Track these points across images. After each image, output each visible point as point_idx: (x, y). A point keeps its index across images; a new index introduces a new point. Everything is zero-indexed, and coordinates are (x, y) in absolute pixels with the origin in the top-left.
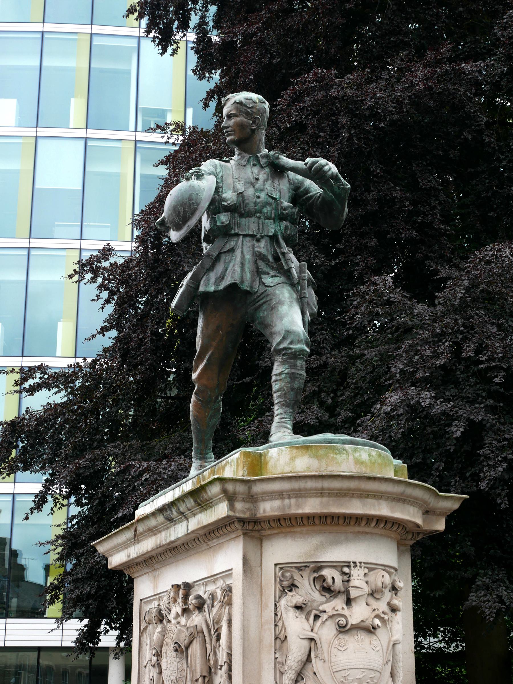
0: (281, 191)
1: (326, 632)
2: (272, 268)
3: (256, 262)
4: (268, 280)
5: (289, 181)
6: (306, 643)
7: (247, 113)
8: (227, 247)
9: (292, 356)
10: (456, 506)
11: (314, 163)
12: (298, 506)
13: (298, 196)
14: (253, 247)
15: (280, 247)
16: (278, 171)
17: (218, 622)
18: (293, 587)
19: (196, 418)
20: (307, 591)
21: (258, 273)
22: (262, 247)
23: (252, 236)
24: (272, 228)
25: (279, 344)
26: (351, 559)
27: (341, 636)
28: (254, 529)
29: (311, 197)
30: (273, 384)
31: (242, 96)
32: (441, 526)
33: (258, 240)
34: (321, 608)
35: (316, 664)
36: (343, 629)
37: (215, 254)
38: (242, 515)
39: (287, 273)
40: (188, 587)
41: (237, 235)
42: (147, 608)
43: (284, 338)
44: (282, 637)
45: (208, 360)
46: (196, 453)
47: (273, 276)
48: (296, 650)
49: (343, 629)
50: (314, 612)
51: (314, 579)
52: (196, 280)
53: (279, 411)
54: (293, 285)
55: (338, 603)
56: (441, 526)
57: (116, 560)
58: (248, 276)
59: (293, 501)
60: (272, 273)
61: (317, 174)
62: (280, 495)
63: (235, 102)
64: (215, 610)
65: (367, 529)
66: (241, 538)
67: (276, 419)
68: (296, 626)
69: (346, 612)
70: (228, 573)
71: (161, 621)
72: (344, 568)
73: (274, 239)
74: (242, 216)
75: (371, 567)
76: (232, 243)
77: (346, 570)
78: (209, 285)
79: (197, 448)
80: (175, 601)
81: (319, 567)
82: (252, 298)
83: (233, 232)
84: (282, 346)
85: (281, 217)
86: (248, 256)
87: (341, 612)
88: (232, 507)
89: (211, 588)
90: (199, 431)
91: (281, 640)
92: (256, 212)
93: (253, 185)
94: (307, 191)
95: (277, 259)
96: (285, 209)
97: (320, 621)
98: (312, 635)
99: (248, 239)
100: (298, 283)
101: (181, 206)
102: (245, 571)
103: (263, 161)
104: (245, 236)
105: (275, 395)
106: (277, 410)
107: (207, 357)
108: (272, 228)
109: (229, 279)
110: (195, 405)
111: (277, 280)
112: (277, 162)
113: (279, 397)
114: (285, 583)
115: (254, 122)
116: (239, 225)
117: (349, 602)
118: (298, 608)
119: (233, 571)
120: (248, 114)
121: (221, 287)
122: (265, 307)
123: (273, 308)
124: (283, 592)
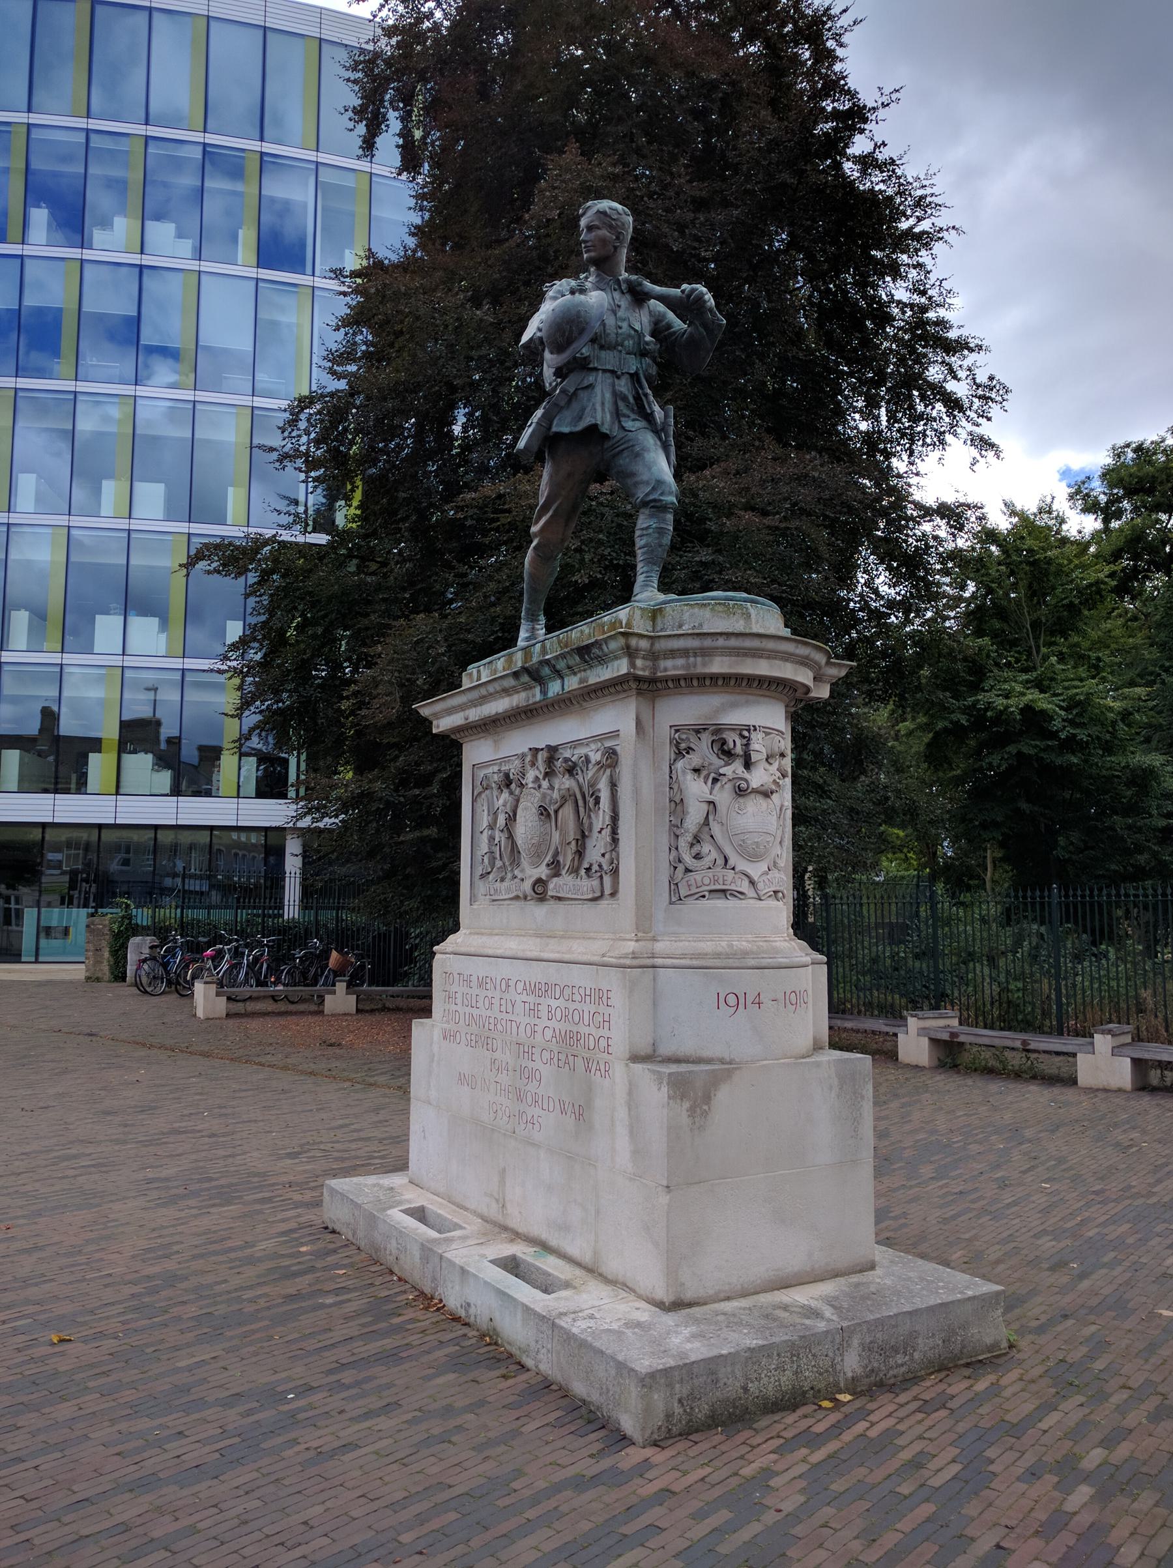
0: (641, 321)
1: (723, 796)
2: (633, 411)
3: (616, 403)
4: (629, 424)
5: (650, 312)
6: (705, 807)
7: (611, 226)
8: (586, 383)
10: (843, 673)
11: (693, 290)
12: (704, 665)
13: (659, 329)
14: (613, 385)
15: (642, 388)
16: (639, 297)
17: (592, 785)
18: (689, 750)
19: (531, 575)
20: (703, 751)
21: (617, 415)
22: (623, 386)
23: (613, 372)
24: (633, 365)
25: (647, 495)
26: (751, 723)
27: (741, 800)
28: (649, 687)
29: (675, 333)
30: (637, 540)
31: (605, 204)
33: (618, 378)
34: (721, 771)
37: (572, 390)
38: (641, 673)
39: (649, 417)
40: (552, 750)
41: (596, 369)
42: (481, 774)
43: (654, 489)
44: (678, 800)
45: (555, 511)
46: (527, 613)
47: (634, 420)
49: (741, 792)
50: (712, 775)
51: (713, 742)
52: (548, 418)
53: (645, 569)
55: (737, 768)
57: (442, 725)
59: (699, 659)
60: (633, 416)
61: (682, 307)
62: (685, 653)
63: (598, 211)
64: (590, 774)
65: (768, 693)
66: (634, 698)
67: (640, 579)
68: (696, 789)
69: (746, 775)
70: (615, 734)
71: (508, 786)
72: (743, 733)
73: (634, 377)
74: (602, 347)
76: (591, 379)
77: (746, 733)
78: (563, 426)
79: (528, 610)
80: (533, 764)
81: (718, 730)
82: (611, 443)
83: (591, 366)
84: (651, 497)
85: (643, 353)
86: (608, 396)
87: (742, 775)
88: (632, 665)
89: (582, 751)
90: (534, 590)
91: (678, 804)
92: (617, 344)
94: (669, 326)
95: (637, 398)
96: (647, 343)
97: (719, 784)
98: (711, 798)
99: (608, 375)
100: (663, 429)
101: (568, 323)
102: (638, 733)
103: (624, 286)
104: (605, 371)
105: (639, 552)
107: (553, 508)
108: (633, 365)
109: (588, 419)
110: (532, 562)
111: (638, 424)
112: (638, 288)
113: (644, 554)
114: (683, 746)
115: (618, 238)
116: (598, 358)
117: (748, 765)
118: (696, 771)
119: (621, 733)
121: (579, 428)
122: (625, 454)
123: (637, 455)
124: (680, 754)
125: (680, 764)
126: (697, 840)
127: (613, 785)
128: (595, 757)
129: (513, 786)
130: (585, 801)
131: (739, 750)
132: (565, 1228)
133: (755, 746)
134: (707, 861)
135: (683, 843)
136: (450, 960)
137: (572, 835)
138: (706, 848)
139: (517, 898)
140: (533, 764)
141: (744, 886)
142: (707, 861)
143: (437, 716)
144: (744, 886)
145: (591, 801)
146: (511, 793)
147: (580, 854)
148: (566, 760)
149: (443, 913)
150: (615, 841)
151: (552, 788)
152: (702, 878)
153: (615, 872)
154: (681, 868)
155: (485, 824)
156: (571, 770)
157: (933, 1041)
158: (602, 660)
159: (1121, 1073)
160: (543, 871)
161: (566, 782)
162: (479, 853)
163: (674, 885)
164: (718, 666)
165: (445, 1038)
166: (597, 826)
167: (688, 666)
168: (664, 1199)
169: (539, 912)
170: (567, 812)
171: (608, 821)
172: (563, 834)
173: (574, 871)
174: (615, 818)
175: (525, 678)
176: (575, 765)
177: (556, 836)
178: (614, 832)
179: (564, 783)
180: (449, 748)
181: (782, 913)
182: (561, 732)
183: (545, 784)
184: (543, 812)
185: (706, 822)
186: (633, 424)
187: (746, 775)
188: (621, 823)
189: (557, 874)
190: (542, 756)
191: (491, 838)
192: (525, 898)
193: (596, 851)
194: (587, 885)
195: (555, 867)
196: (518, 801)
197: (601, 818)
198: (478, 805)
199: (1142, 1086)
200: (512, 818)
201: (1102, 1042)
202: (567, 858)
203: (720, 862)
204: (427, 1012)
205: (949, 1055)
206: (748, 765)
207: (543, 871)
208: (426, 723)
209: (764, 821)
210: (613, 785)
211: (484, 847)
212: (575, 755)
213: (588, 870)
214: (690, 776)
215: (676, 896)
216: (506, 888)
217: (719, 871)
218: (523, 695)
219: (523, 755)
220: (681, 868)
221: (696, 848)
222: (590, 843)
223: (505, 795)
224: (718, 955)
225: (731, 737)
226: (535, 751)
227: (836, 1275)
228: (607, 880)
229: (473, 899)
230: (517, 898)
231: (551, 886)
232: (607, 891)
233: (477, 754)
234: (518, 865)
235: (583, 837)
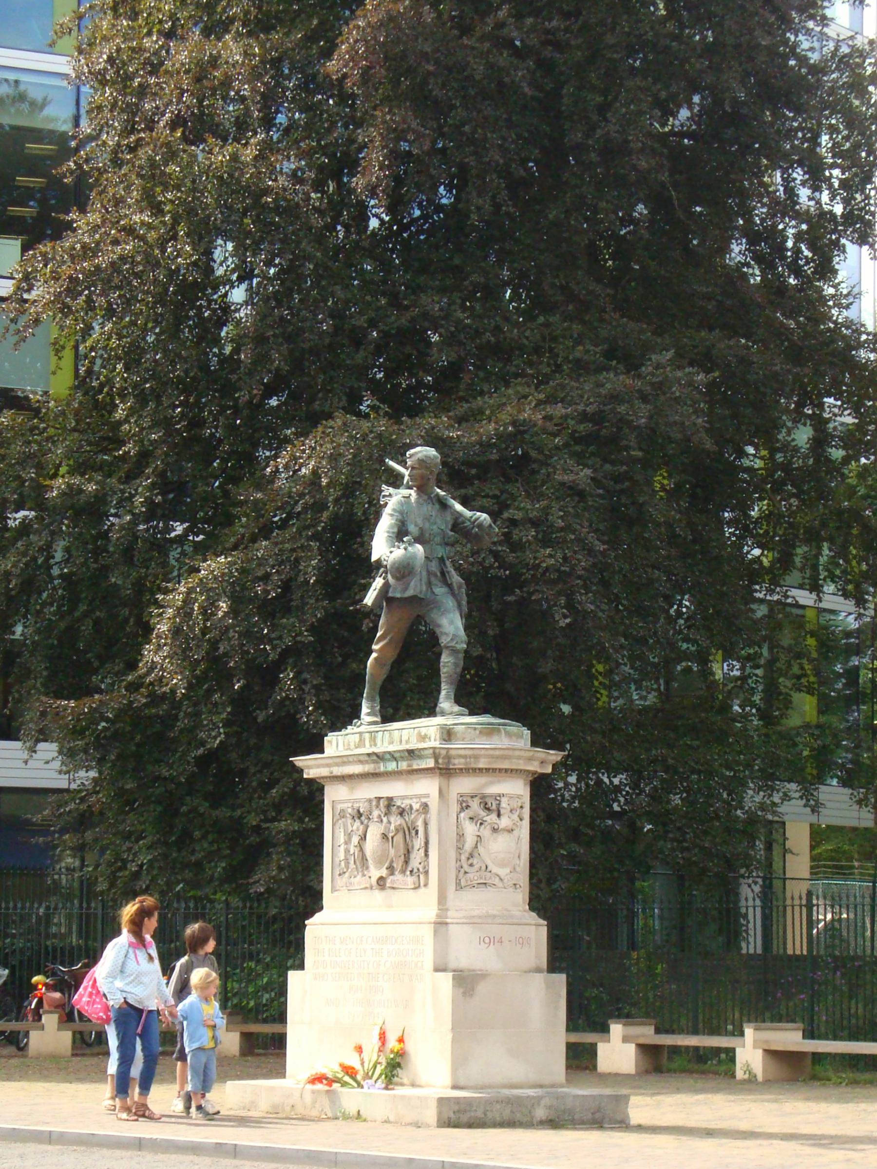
1: (486, 832)
9: (454, 651)
10: (559, 758)
18: (468, 807)
19: (372, 674)
21: (429, 584)
32: (549, 770)
35: (481, 849)
36: (495, 830)
40: (390, 799)
42: (339, 807)
49: (495, 830)
54: (453, 595)
56: (549, 770)
58: (424, 588)
62: (465, 757)
68: (470, 829)
72: (498, 797)
73: (442, 560)
75: (511, 797)
91: (461, 836)
93: (429, 520)
95: (443, 573)
106: (444, 686)
110: (374, 666)
117: (499, 815)
120: (427, 468)
124: (462, 809)
125: (462, 815)
126: (471, 856)
127: (426, 824)
128: (416, 806)
129: (363, 818)
130: (409, 831)
131: (494, 807)
133: (503, 805)
134: (476, 867)
135: (463, 858)
136: (316, 929)
137: (402, 851)
139: (366, 888)
140: (377, 806)
141: (497, 881)
142: (476, 867)
143: (309, 767)
144: (497, 881)
145: (413, 832)
146: (362, 823)
147: (406, 862)
148: (399, 807)
149: (313, 901)
150: (426, 855)
151: (389, 823)
152: (473, 876)
153: (426, 873)
154: (462, 871)
155: (342, 841)
156: (402, 813)
157: (639, 1046)
158: (420, 757)
160: (384, 872)
162: (337, 860)
165: (315, 978)
166: (417, 847)
167: (466, 763)
170: (399, 838)
171: (423, 844)
172: (397, 851)
173: (403, 872)
174: (427, 843)
175: (375, 758)
176: (404, 810)
177: (392, 852)
178: (426, 851)
179: (396, 821)
180: (316, 789)
183: (385, 819)
185: (476, 847)
186: (440, 590)
187: (498, 821)
188: (430, 846)
189: (392, 874)
190: (382, 803)
191: (347, 851)
192: (371, 888)
193: (416, 860)
194: (410, 880)
195: (391, 869)
196: (367, 827)
197: (419, 842)
198: (337, 827)
200: (364, 838)
201: (616, 1029)
202: (398, 865)
203: (484, 868)
204: (301, 967)
206: (499, 815)
207: (384, 872)
208: (300, 771)
209: (509, 847)
210: (426, 824)
211: (341, 855)
212: (405, 804)
213: (411, 871)
214: (467, 822)
215: (459, 887)
216: (359, 881)
217: (483, 873)
218: (372, 766)
219: (370, 801)
220: (462, 871)
221: (470, 861)
222: (412, 856)
223: (357, 823)
224: (480, 917)
225: (489, 801)
226: (379, 799)
227: (541, 1086)
228: (422, 877)
229: (334, 889)
230: (366, 888)
231: (389, 881)
232: (422, 884)
234: (367, 868)
235: (408, 852)
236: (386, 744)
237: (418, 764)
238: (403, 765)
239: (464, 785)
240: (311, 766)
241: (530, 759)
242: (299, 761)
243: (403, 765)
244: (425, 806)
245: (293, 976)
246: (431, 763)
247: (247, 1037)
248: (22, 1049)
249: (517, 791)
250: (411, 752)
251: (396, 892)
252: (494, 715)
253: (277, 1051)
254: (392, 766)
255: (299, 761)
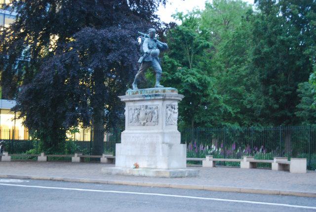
1: (172, 113)
20: (170, 108)
28: (164, 100)
48: (169, 115)
55: (173, 110)
68: (169, 112)
70: (158, 105)
91: (167, 114)
132: (151, 165)
136: (124, 135)
138: (170, 119)
149: (124, 129)
157: (107, 158)
159: (211, 164)
160: (145, 121)
161: (150, 110)
163: (166, 124)
164: (173, 98)
168: (167, 158)
169: (144, 127)
181: (176, 127)
182: (149, 103)
184: (146, 114)
186: (155, 60)
194: (154, 124)
199: (214, 166)
205: (254, 165)
207: (145, 121)
208: (120, 99)
226: (143, 106)
233: (127, 104)
236: (145, 93)
237: (159, 98)
238: (153, 98)
239: (168, 103)
240: (123, 98)
241: (177, 97)
242: (120, 97)
243: (153, 98)
244: (157, 108)
245: (117, 145)
246: (162, 98)
247: (214, 162)
248: (288, 170)
249: (176, 104)
250: (156, 95)
251: (149, 126)
252: (172, 87)
253: (200, 165)
254: (149, 98)
255: (120, 97)
